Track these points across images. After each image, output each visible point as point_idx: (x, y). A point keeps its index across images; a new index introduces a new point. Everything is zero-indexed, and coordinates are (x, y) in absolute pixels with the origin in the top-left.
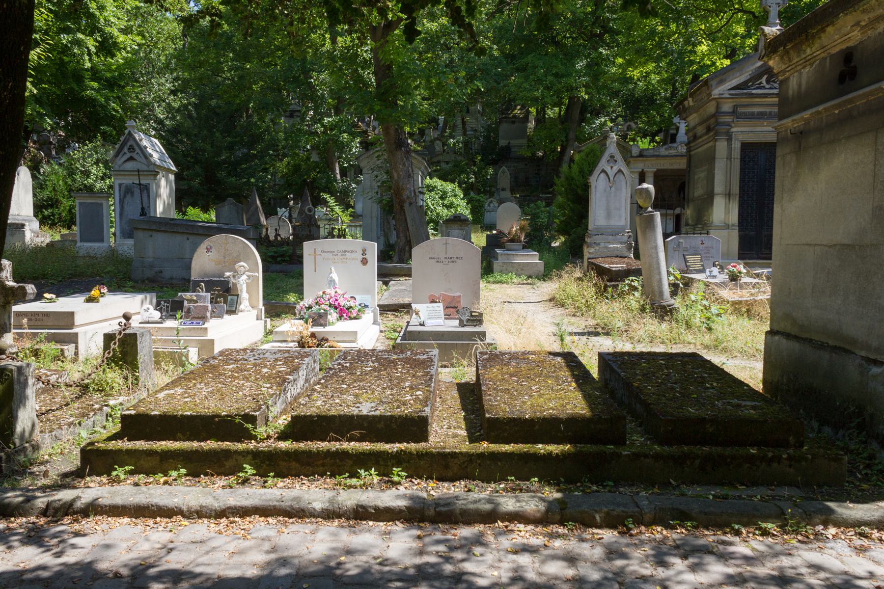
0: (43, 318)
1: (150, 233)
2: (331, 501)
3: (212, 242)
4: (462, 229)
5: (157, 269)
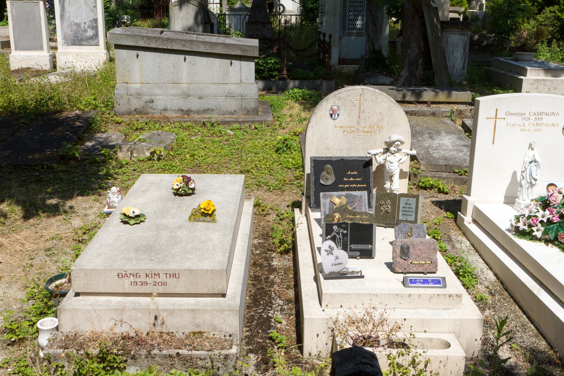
0: (168, 280)
1: (135, 52)
2: (130, 220)
3: (340, 99)
4: (463, 35)
5: (146, 98)
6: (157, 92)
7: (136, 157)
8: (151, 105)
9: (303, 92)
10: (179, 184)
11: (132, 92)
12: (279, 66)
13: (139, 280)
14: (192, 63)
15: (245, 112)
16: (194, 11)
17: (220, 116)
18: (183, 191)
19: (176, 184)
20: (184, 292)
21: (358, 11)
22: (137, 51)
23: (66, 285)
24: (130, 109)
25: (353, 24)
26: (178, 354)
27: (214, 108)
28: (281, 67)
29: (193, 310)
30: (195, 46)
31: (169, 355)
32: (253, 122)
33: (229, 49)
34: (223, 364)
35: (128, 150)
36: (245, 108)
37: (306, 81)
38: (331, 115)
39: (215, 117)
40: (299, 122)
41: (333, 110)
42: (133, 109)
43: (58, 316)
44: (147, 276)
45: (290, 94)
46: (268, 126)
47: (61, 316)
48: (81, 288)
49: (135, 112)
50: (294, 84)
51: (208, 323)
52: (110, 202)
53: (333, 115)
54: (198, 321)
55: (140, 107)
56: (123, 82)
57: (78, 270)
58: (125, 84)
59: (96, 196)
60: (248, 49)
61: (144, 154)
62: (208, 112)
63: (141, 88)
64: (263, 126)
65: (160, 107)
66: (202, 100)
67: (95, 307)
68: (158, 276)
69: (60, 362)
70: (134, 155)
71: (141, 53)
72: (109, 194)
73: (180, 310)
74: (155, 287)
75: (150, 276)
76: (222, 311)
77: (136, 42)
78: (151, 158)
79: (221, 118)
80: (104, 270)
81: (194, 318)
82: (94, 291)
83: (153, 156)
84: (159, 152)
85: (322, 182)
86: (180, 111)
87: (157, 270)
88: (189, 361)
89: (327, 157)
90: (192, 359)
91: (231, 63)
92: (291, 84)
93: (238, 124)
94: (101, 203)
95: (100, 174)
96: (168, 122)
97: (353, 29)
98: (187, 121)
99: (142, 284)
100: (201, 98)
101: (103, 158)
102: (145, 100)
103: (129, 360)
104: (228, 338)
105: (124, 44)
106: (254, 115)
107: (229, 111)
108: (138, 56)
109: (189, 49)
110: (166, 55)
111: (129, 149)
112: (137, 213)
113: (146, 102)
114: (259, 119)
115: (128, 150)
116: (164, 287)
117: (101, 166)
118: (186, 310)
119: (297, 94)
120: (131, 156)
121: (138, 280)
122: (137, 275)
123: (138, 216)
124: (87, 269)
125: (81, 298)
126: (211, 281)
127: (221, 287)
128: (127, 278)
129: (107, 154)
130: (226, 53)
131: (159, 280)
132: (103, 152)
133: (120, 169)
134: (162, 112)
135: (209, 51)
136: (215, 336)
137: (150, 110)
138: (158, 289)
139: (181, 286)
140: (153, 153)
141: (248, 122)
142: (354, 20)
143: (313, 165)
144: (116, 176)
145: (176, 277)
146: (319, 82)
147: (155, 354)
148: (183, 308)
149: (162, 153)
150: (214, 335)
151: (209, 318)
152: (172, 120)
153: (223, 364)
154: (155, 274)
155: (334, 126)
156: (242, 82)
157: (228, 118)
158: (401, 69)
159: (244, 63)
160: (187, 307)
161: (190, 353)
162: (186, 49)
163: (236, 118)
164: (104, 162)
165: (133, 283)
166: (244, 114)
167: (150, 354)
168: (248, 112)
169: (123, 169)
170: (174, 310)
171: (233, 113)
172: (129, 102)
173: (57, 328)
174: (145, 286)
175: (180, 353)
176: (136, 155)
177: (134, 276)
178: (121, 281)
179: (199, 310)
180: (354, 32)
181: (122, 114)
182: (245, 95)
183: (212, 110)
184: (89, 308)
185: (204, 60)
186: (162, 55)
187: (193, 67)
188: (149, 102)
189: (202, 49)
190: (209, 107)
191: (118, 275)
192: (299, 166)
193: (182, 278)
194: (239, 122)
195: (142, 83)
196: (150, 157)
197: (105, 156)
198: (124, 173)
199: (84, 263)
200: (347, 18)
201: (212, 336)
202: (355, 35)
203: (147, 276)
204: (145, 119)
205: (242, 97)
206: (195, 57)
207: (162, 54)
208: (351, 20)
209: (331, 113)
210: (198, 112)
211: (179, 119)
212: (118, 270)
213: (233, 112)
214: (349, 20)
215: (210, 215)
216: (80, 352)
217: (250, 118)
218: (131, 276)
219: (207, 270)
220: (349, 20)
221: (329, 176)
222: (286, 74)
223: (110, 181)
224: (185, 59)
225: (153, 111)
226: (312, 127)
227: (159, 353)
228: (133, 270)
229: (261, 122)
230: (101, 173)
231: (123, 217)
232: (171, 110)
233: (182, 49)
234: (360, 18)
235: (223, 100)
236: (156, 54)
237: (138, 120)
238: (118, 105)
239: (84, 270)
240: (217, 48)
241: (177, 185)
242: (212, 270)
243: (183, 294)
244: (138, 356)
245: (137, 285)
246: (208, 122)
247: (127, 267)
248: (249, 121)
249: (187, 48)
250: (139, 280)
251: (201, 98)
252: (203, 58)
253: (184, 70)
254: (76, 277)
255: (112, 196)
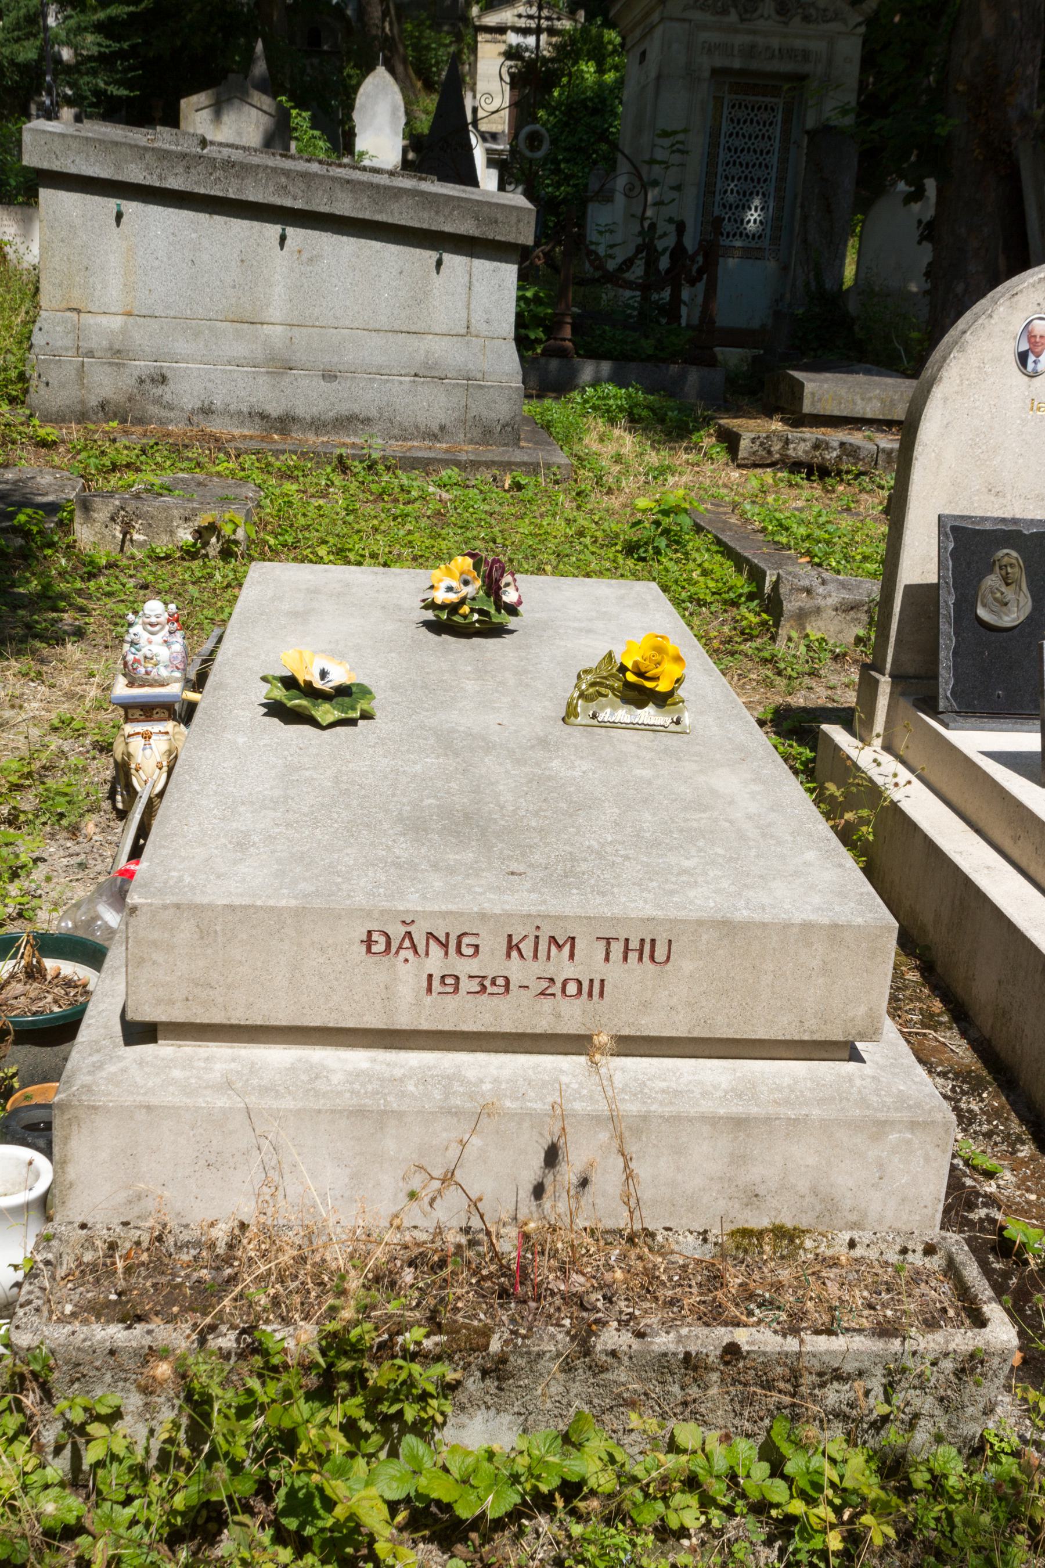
5: (143, 366)
6: (182, 346)
7: (141, 545)
8: (158, 391)
9: (629, 396)
10: (455, 584)
11: (94, 342)
12: (550, 311)
13: (473, 966)
14: (305, 256)
15: (476, 433)
16: (261, 129)
17: (392, 442)
18: (476, 617)
19: (443, 586)
20: (682, 1032)
21: (752, 180)
22: (119, 201)
23: (17, 988)
24: (82, 402)
25: (736, 221)
26: (732, 1351)
27: (374, 413)
28: (555, 315)
29: (739, 1123)
30: (320, 193)
31: (688, 1355)
32: (508, 466)
33: (437, 213)
34: (941, 1400)
35: (113, 519)
36: (477, 420)
37: (633, 365)
38: (1023, 358)
39: (378, 446)
40: (655, 478)
41: (1031, 337)
42: (93, 402)
43: (56, 1149)
44: (510, 948)
45: (586, 401)
46: (557, 482)
47: (74, 1143)
48: (172, 1002)
49: (101, 414)
50: (597, 371)
51: (803, 1185)
52: (136, 661)
53: (1031, 358)
54: (754, 1173)
55: (121, 398)
56: (64, 305)
57: (165, 907)
58: (68, 314)
59: (26, 663)
60: (500, 217)
61: (172, 533)
62: (352, 426)
63: (124, 331)
64: (541, 480)
65: (190, 403)
66: (335, 385)
67: (252, 1100)
68: (567, 948)
69: (99, 1392)
70: (136, 536)
71: (131, 208)
72: (132, 630)
73: (676, 1120)
74: (547, 1003)
75: (527, 947)
76: (879, 1127)
77: (118, 167)
78: (198, 551)
79: (396, 448)
80: (299, 913)
81: (738, 1159)
82: (238, 1017)
83: (206, 544)
84: (231, 526)
85: (981, 612)
86: (257, 419)
87: (566, 918)
88: (781, 1385)
89: (1003, 520)
90: (795, 1376)
91: (439, 263)
92: (588, 371)
93: (456, 470)
94: (52, 686)
95: (20, 594)
96: (219, 450)
97: (734, 235)
98: (283, 452)
99: (484, 988)
100: (329, 376)
101: (20, 541)
102: (136, 373)
103: (473, 1384)
104: (917, 1259)
105: (73, 170)
106: (506, 445)
107: (423, 428)
108: (119, 216)
109: (299, 205)
110: (219, 221)
111: (117, 514)
112: (339, 676)
113: (142, 381)
114: (526, 459)
115: (113, 519)
116: (590, 1006)
117: (16, 568)
118: (704, 1118)
119: (611, 402)
120: (123, 541)
121: (464, 967)
122: (466, 940)
123: (343, 691)
124: (211, 907)
125: (163, 1050)
126: (821, 980)
127: (862, 1010)
128: (409, 954)
129: (35, 529)
130: (425, 226)
131: (569, 971)
132: (22, 518)
133: (89, 580)
134: (195, 419)
135: (367, 215)
136: (859, 1252)
137: (153, 410)
138: (559, 1016)
139: (674, 1001)
140: (202, 534)
141: (489, 464)
142: (737, 207)
143: (951, 546)
144: (80, 601)
145: (652, 958)
146: (674, 369)
147: (613, 1354)
148: (692, 1112)
149: (240, 535)
150: (852, 1244)
151: (811, 1160)
152: (232, 444)
153: (941, 1400)
154: (553, 939)
155: (1028, 401)
156: (472, 330)
157: (419, 448)
158: (926, 344)
159: (482, 266)
160: (707, 1107)
161: (791, 1344)
162: (288, 203)
163: (447, 451)
164: (25, 557)
165: (436, 983)
166: (471, 441)
167: (587, 1353)
168: (486, 434)
169: (103, 580)
170: (645, 1118)
171: (435, 436)
172: (82, 379)
173: (44, 1205)
174: (496, 1000)
175: (745, 1348)
176: (142, 538)
177: (445, 946)
178: (378, 970)
179: (768, 1120)
180: (738, 243)
181: (57, 419)
182: (479, 376)
183: (367, 421)
184: (222, 1102)
185: (348, 246)
186: (202, 218)
187: (309, 269)
188: (153, 380)
189: (344, 206)
190: (356, 408)
191: (369, 942)
192: (740, 596)
193: (684, 964)
194: (458, 464)
195: (129, 314)
196: (194, 545)
197: (27, 534)
198: (109, 594)
199: (187, 879)
200: (718, 198)
201: (844, 1250)
202: (737, 253)
203: (512, 946)
204: (136, 437)
205: (470, 383)
206: (317, 233)
207: (203, 217)
208: (731, 206)
209: (1024, 346)
210: (318, 425)
211: (254, 445)
212: (369, 914)
213: (436, 429)
214: (724, 206)
215: (662, 700)
216: (215, 1343)
217: (495, 453)
218: (433, 946)
219: (807, 927)
220: (724, 206)
221: (1009, 593)
222: (569, 337)
223: (65, 616)
224: (283, 239)
225: (164, 413)
226: (945, 400)
227: (636, 1344)
228: (444, 915)
229: (533, 468)
230: (21, 590)
231: (279, 693)
232: (226, 412)
233: (278, 201)
234: (757, 202)
235: (406, 387)
236: (185, 213)
237: (114, 441)
238: (42, 386)
239: (196, 909)
240: (395, 206)
241: (450, 589)
242: (836, 926)
243: (670, 1040)
244: (521, 1362)
245: (456, 990)
246: (354, 457)
247: (411, 902)
248: (493, 463)
249: (295, 198)
250: (473, 966)
251: (329, 376)
252: (345, 239)
253: (277, 277)
254: (154, 944)
255: (144, 636)
